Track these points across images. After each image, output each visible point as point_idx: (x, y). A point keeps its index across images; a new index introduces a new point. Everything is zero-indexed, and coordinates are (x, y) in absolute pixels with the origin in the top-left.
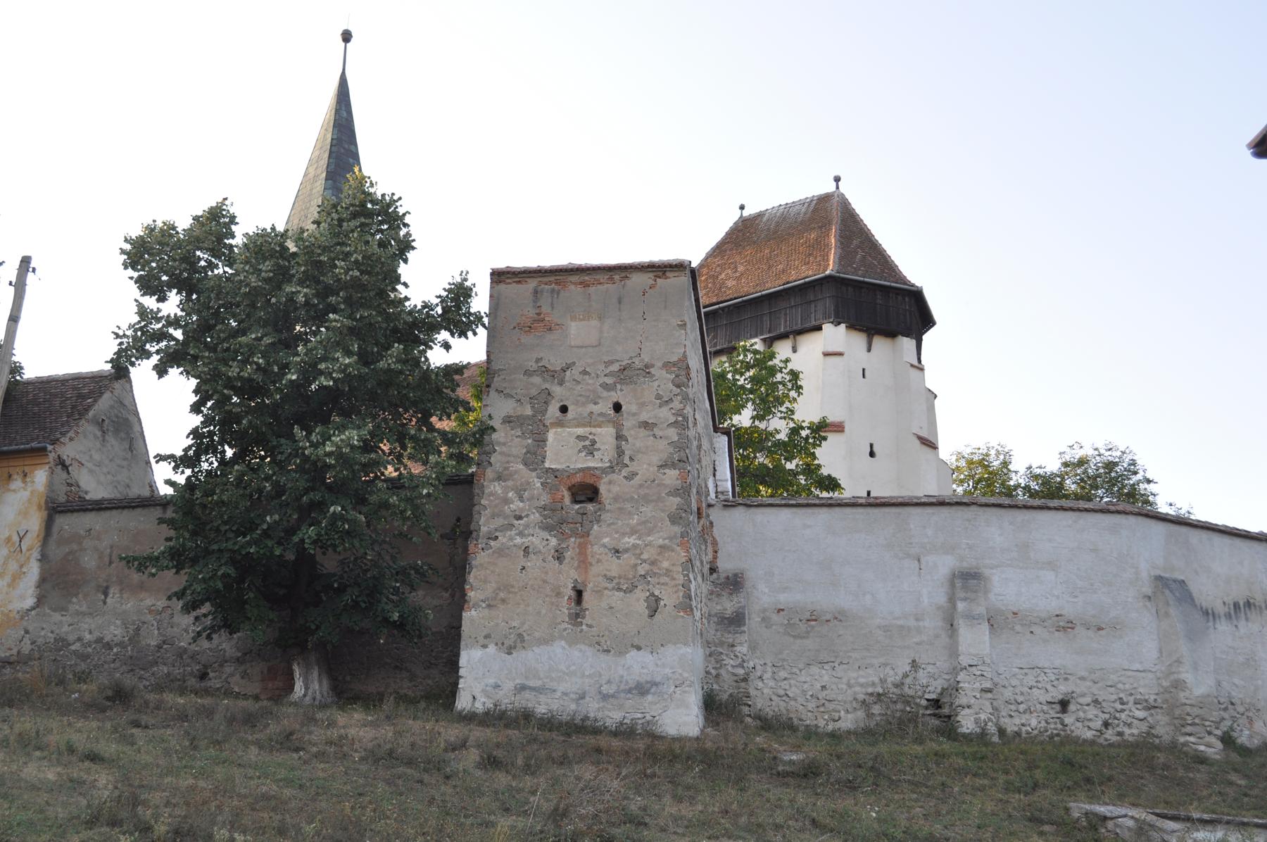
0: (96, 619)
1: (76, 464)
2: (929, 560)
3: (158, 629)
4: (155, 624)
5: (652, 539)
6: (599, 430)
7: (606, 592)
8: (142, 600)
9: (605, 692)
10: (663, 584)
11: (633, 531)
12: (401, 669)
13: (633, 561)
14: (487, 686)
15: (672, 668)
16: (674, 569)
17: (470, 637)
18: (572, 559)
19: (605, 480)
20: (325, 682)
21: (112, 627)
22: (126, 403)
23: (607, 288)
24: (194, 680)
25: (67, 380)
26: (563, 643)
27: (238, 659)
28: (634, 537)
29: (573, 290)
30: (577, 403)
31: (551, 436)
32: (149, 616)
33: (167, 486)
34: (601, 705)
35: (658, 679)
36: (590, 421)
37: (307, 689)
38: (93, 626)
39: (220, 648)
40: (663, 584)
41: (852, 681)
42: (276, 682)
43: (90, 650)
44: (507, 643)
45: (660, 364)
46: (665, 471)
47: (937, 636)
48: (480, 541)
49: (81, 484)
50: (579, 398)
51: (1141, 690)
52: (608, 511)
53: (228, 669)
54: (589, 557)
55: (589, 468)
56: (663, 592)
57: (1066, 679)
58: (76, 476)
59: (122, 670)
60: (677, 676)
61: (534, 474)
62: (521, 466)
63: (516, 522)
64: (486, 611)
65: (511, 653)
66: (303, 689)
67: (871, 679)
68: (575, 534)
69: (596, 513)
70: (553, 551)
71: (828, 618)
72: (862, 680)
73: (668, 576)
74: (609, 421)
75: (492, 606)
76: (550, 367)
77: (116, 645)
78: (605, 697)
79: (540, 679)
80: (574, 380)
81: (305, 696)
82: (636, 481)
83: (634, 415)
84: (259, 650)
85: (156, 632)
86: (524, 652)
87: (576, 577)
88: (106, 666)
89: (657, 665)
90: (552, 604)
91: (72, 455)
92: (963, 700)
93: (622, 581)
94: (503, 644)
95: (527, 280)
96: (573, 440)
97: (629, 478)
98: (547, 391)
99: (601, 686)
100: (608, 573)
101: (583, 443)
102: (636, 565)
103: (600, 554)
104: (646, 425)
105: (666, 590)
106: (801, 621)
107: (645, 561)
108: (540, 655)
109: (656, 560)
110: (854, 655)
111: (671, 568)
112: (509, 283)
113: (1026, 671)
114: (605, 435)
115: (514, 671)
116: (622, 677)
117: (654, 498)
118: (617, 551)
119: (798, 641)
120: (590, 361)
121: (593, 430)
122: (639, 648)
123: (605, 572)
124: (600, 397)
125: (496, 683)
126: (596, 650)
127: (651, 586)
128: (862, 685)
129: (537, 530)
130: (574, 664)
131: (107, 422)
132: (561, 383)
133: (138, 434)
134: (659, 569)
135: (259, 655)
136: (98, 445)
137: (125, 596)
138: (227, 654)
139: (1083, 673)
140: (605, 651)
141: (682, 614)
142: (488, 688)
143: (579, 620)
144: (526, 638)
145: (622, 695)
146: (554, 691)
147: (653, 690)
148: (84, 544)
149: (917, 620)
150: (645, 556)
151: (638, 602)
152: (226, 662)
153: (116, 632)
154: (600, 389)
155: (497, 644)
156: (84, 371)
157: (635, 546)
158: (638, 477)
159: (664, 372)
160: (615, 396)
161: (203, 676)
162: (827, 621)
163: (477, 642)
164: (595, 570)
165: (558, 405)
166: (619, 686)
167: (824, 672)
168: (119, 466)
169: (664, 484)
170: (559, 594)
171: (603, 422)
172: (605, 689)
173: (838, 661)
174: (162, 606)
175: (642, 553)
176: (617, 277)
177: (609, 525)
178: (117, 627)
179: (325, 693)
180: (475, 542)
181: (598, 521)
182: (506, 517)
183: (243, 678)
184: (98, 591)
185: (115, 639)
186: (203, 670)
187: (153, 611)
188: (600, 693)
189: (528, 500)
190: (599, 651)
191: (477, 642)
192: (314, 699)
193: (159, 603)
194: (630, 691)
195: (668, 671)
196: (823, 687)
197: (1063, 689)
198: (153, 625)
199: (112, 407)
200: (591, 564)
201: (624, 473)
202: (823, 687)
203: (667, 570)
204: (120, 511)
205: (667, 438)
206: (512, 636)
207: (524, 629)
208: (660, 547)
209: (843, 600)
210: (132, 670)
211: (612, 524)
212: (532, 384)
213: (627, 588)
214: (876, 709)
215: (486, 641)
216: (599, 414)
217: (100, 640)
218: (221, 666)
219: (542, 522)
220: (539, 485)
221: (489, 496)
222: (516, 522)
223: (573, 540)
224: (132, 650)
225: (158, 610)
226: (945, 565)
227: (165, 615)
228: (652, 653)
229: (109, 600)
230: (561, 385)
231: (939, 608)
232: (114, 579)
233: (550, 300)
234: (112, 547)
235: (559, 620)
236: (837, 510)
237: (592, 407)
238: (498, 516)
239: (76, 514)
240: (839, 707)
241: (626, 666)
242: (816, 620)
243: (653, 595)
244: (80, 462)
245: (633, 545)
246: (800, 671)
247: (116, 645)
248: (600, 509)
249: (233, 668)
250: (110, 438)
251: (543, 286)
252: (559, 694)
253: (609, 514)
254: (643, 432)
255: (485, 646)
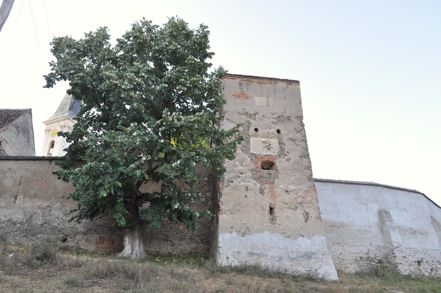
0: (9, 210)
1: (4, 142)
2: (370, 205)
3: (43, 216)
4: (41, 214)
5: (301, 187)
6: (271, 140)
7: (285, 209)
8: (35, 202)
9: (291, 257)
10: (309, 207)
11: (293, 183)
12: (167, 241)
13: (295, 196)
14: (234, 252)
15: (319, 246)
16: (313, 201)
17: (223, 227)
18: (268, 193)
19: (277, 161)
20: (142, 247)
21: (17, 215)
22: (29, 122)
23: (267, 86)
24: (59, 242)
25: (2, 111)
26: (268, 232)
27: (84, 233)
28: (293, 186)
29: (255, 85)
30: (262, 128)
31: (252, 140)
32: (38, 210)
33: (209, 63)
34: (291, 263)
35: (314, 251)
36: (268, 136)
37: (133, 250)
38: (7, 214)
39: (75, 227)
40: (309, 207)
41: (351, 252)
42: (104, 245)
43: (4, 225)
44: (242, 231)
45: (294, 117)
46: (302, 159)
47: (377, 235)
48: (224, 182)
49: (6, 151)
50: (262, 126)
51: (437, 257)
52: (281, 174)
53: (78, 237)
54: (275, 193)
55: (270, 155)
56: (310, 211)
57: (417, 253)
58: (4, 147)
59: (20, 235)
60: (322, 250)
61: (247, 155)
62: (241, 151)
63: (241, 175)
64: (230, 215)
65: (244, 236)
66: (130, 250)
67: (357, 251)
68: (267, 182)
69: (275, 174)
70: (259, 189)
71: (338, 226)
72: (354, 251)
73: (311, 204)
74: (276, 137)
75: (233, 213)
76: (249, 113)
77: (19, 223)
78: (292, 259)
79: (259, 249)
80: (260, 119)
81: (132, 254)
82: (291, 162)
83: (286, 135)
84: (96, 229)
85: (41, 218)
86: (250, 236)
87: (270, 202)
88: (12, 233)
89: (312, 244)
90: (261, 213)
91: (3, 138)
92: (399, 261)
93: (291, 204)
94: (240, 231)
95: (236, 78)
96: (260, 143)
97: (288, 160)
98: (248, 122)
99: (289, 254)
100: (284, 201)
101: (265, 145)
102: (296, 198)
103: (280, 192)
104: (291, 139)
105: (311, 210)
106: (329, 226)
107: (300, 196)
108: (258, 237)
109: (305, 196)
110: (350, 241)
111: (311, 200)
112: (229, 79)
113: (406, 249)
114: (274, 142)
115: (246, 245)
116: (298, 249)
117: (300, 169)
118: (287, 192)
119: (329, 234)
120: (266, 112)
121: (269, 140)
122: (303, 236)
123: (283, 200)
124: (271, 127)
125: (238, 251)
126: (283, 237)
127: (304, 208)
128: (354, 253)
129: (251, 180)
130: (274, 243)
131: (20, 128)
132: (254, 119)
133: (31, 137)
134: (307, 200)
135: (95, 231)
136: (15, 136)
137: (26, 200)
138: (79, 230)
139: (421, 251)
140: (287, 237)
141: (319, 221)
142: (234, 253)
143: (274, 222)
144: (251, 229)
145: (300, 259)
146: (267, 256)
147: (313, 256)
148: (6, 175)
149: (370, 228)
150: (299, 194)
151: (299, 214)
152: (78, 234)
153: (19, 217)
154: (271, 123)
155: (237, 232)
156: (21, 108)
157: (295, 190)
158: (291, 160)
159: (296, 120)
160: (277, 127)
161: (65, 240)
162: (338, 227)
163: (227, 230)
164: (278, 199)
165: (254, 128)
166: (297, 254)
167: (340, 247)
168: (22, 147)
169: (303, 164)
170: (263, 209)
171: (273, 136)
172: (291, 255)
173: (344, 243)
174: (46, 205)
175: (298, 193)
176: (272, 82)
177: (282, 180)
178: (20, 214)
179: (142, 253)
180: (222, 183)
181: (277, 178)
182: (236, 173)
183: (86, 242)
184: (12, 197)
185: (18, 220)
186: (64, 237)
187: (40, 208)
188: (289, 257)
189: (245, 166)
190: (285, 236)
191: (227, 230)
192: (137, 255)
193: (44, 204)
194: (303, 257)
195: (317, 247)
196: (341, 254)
197: (418, 257)
198: (40, 214)
199: (23, 123)
200: (276, 196)
201: (286, 158)
202: (341, 254)
203: (310, 201)
204: (27, 161)
205: (301, 145)
206: (244, 228)
207: (249, 225)
208: (306, 191)
209: (342, 219)
210: (26, 236)
211: (284, 179)
212: (242, 118)
213: (294, 208)
214: (361, 263)
215: (231, 230)
216: (272, 133)
217: (10, 220)
218: (75, 235)
219: (252, 176)
220: (249, 160)
221: (227, 163)
222: (240, 175)
223: (267, 185)
224: (27, 226)
225: (43, 208)
226: (375, 208)
227: (47, 211)
228: (309, 238)
229: (17, 201)
230: (255, 120)
231: (376, 224)
232: (21, 192)
233: (246, 87)
234: (21, 177)
235: (265, 221)
236: (335, 184)
237: (268, 130)
238: (232, 172)
239: (4, 161)
240: (348, 262)
241: (298, 245)
242: (334, 226)
243: (305, 212)
244: (6, 141)
245: (294, 189)
246: (331, 247)
247: (19, 223)
248: (277, 173)
249: (81, 237)
250: (20, 134)
251: (243, 81)
252: (269, 257)
253: (282, 175)
254: (291, 142)
255: (231, 232)
